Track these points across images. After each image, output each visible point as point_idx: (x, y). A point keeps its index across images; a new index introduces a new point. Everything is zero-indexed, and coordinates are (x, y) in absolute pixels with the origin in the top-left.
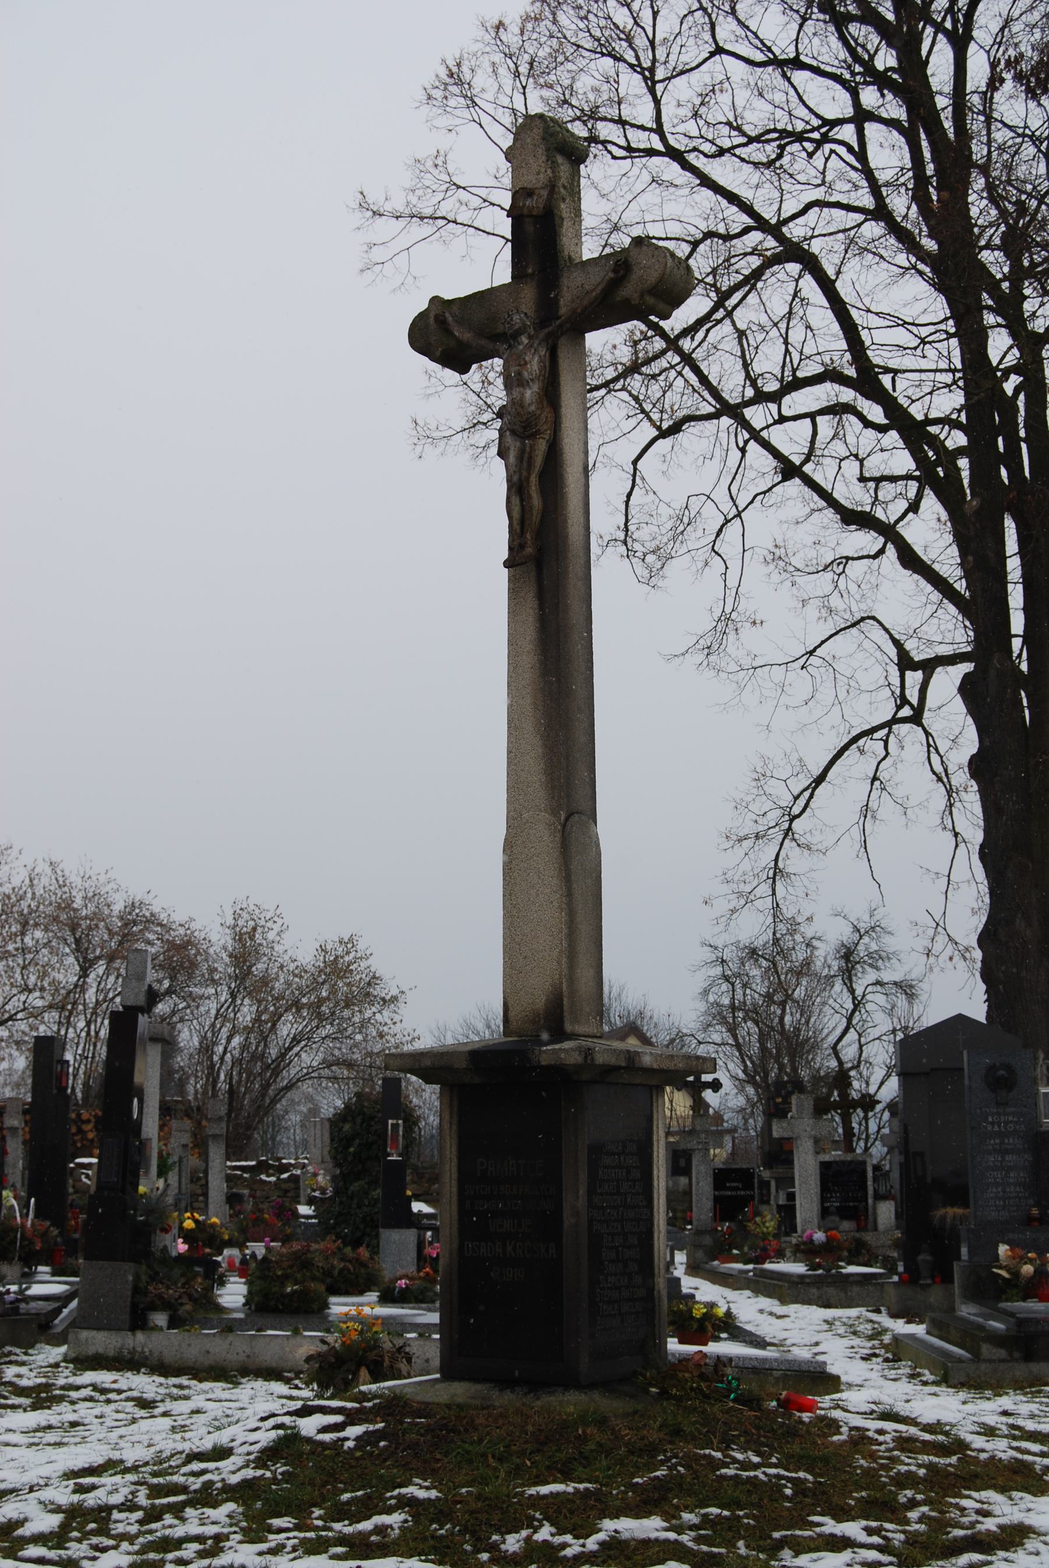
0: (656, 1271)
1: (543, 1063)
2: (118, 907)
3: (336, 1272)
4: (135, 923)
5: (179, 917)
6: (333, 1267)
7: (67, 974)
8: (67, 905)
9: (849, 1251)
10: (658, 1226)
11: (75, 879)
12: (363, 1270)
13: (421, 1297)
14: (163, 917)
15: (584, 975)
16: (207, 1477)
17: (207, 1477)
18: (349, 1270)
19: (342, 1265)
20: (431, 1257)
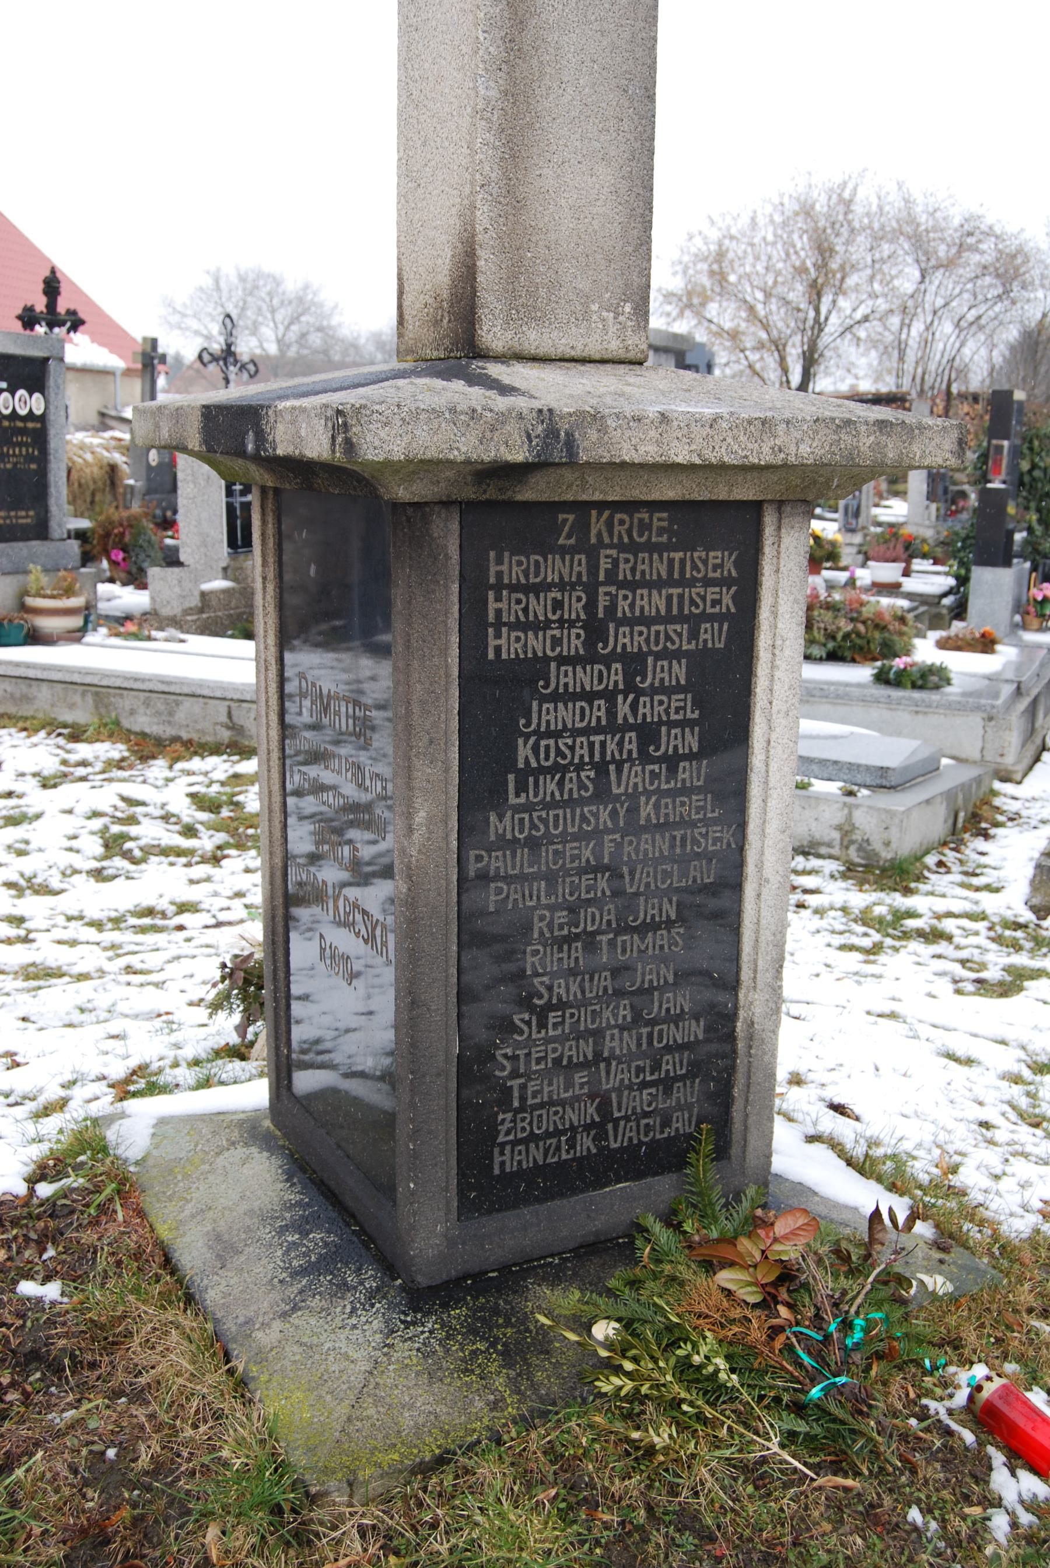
0: (745, 975)
1: (280, 452)
2: (956, 222)
3: (839, 636)
4: (970, 237)
5: (1011, 229)
6: (839, 629)
7: (907, 280)
8: (912, 220)
9: (829, 1520)
10: (760, 867)
11: (917, 196)
12: (877, 635)
13: (920, 682)
14: (998, 230)
15: (572, 191)
16: (627, 878)
17: (627, 878)
18: (858, 634)
19: (850, 627)
20: (1035, 600)
